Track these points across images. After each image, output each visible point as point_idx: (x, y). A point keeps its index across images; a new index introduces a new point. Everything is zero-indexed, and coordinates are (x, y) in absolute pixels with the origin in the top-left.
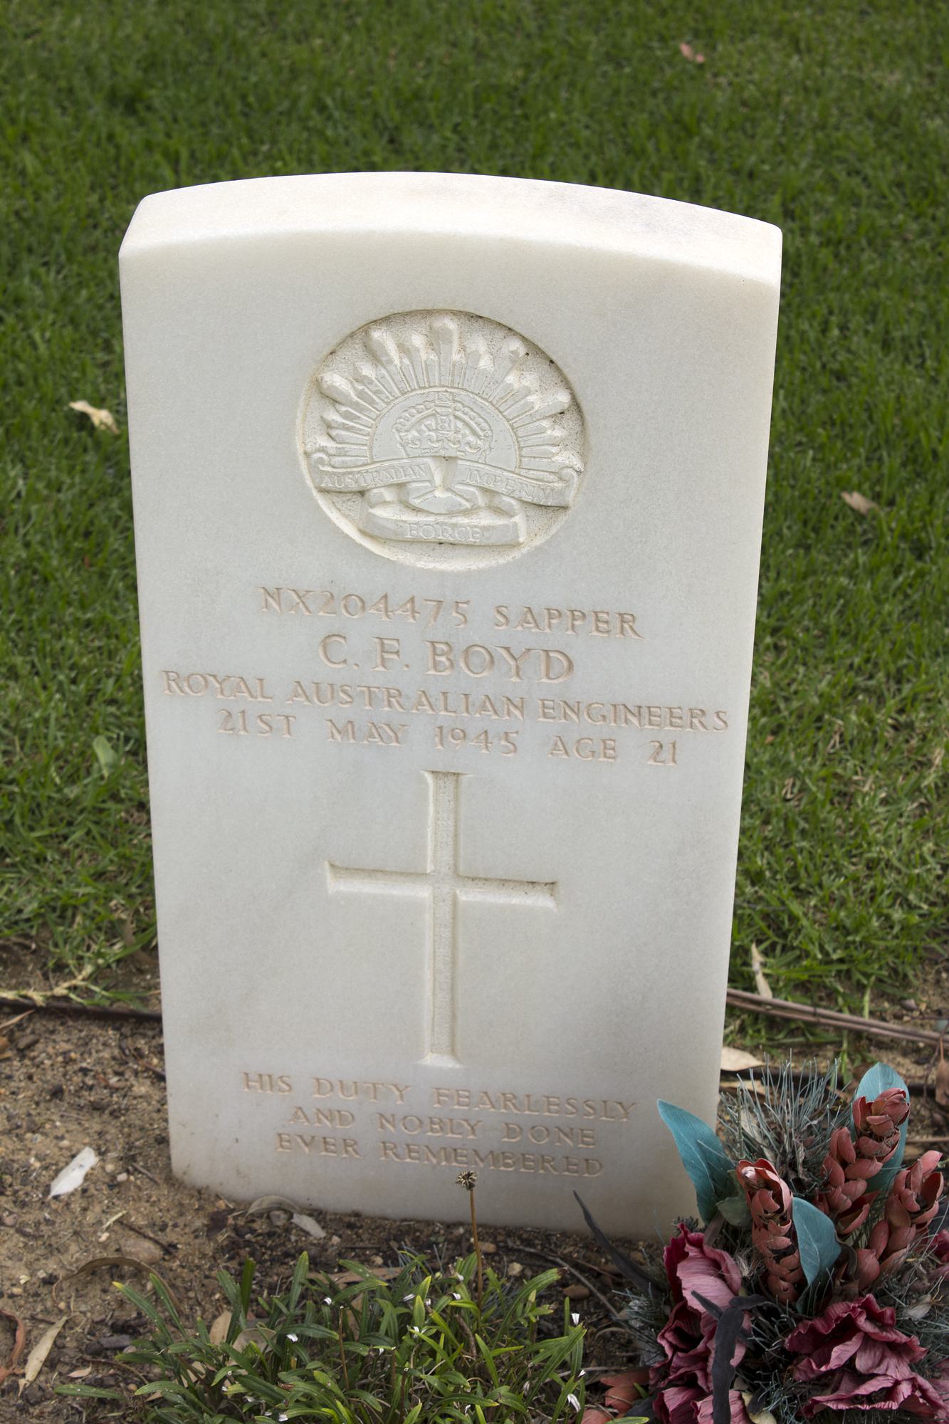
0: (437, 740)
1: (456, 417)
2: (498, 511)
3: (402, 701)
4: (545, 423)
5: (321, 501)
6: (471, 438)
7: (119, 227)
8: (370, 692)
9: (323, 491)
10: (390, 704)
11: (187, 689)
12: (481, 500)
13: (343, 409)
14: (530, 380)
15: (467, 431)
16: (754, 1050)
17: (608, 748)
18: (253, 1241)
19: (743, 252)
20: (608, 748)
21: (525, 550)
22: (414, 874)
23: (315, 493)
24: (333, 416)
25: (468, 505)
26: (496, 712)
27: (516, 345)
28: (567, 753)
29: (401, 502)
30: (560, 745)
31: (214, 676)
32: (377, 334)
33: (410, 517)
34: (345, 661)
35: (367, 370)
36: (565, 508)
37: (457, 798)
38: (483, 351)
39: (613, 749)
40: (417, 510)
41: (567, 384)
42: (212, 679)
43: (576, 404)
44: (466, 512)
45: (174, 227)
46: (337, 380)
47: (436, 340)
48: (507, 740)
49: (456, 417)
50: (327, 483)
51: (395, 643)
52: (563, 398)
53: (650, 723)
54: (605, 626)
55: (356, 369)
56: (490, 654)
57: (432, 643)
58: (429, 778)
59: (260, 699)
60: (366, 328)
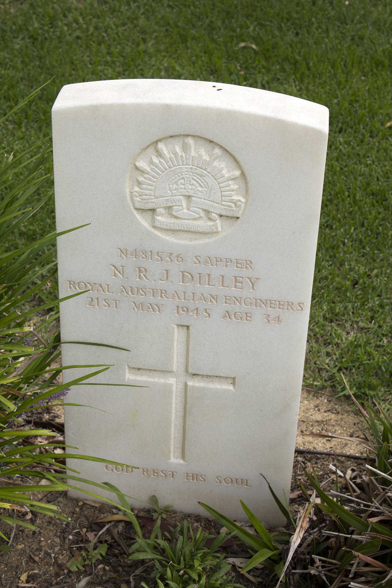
0: (176, 311)
1: (193, 179)
2: (210, 219)
3: (167, 296)
4: (230, 182)
5: (135, 212)
6: (200, 189)
7: (52, 100)
8: (153, 292)
9: (136, 209)
10: (161, 297)
11: (130, 293)
12: (202, 214)
13: (146, 176)
14: (223, 165)
15: (198, 185)
16: (5, 522)
17: (248, 316)
18: (92, 516)
19: (314, 116)
20: (248, 316)
21: (220, 236)
22: (166, 372)
23: (133, 210)
24: (141, 179)
25: (197, 216)
26: (205, 301)
27: (217, 151)
28: (230, 318)
29: (169, 214)
30: (227, 314)
31: (89, 283)
32: (161, 146)
33: (173, 220)
34: (228, 287)
35: (156, 160)
36: (238, 218)
37: (188, 337)
38: (202, 153)
39: (250, 317)
40: (177, 218)
41: (240, 167)
42: (88, 285)
43: (243, 174)
44: (195, 219)
45: (73, 98)
46: (142, 164)
47: (185, 148)
48: (206, 312)
49: (193, 179)
50: (138, 206)
51: (241, 279)
52: (237, 173)
53: (270, 307)
54: (240, 265)
55: (151, 158)
56: (191, 275)
57: (235, 277)
58: (175, 326)
59: (107, 293)
60: (157, 142)
